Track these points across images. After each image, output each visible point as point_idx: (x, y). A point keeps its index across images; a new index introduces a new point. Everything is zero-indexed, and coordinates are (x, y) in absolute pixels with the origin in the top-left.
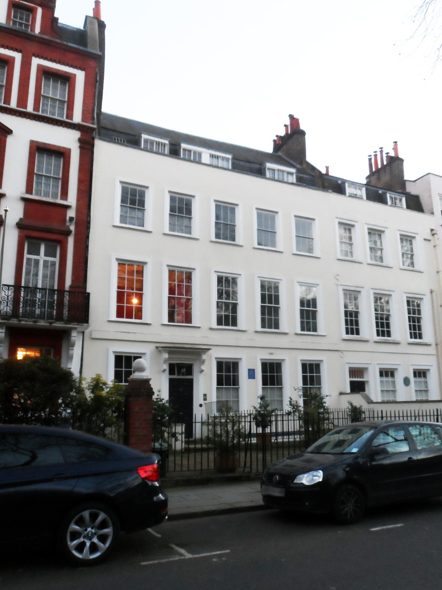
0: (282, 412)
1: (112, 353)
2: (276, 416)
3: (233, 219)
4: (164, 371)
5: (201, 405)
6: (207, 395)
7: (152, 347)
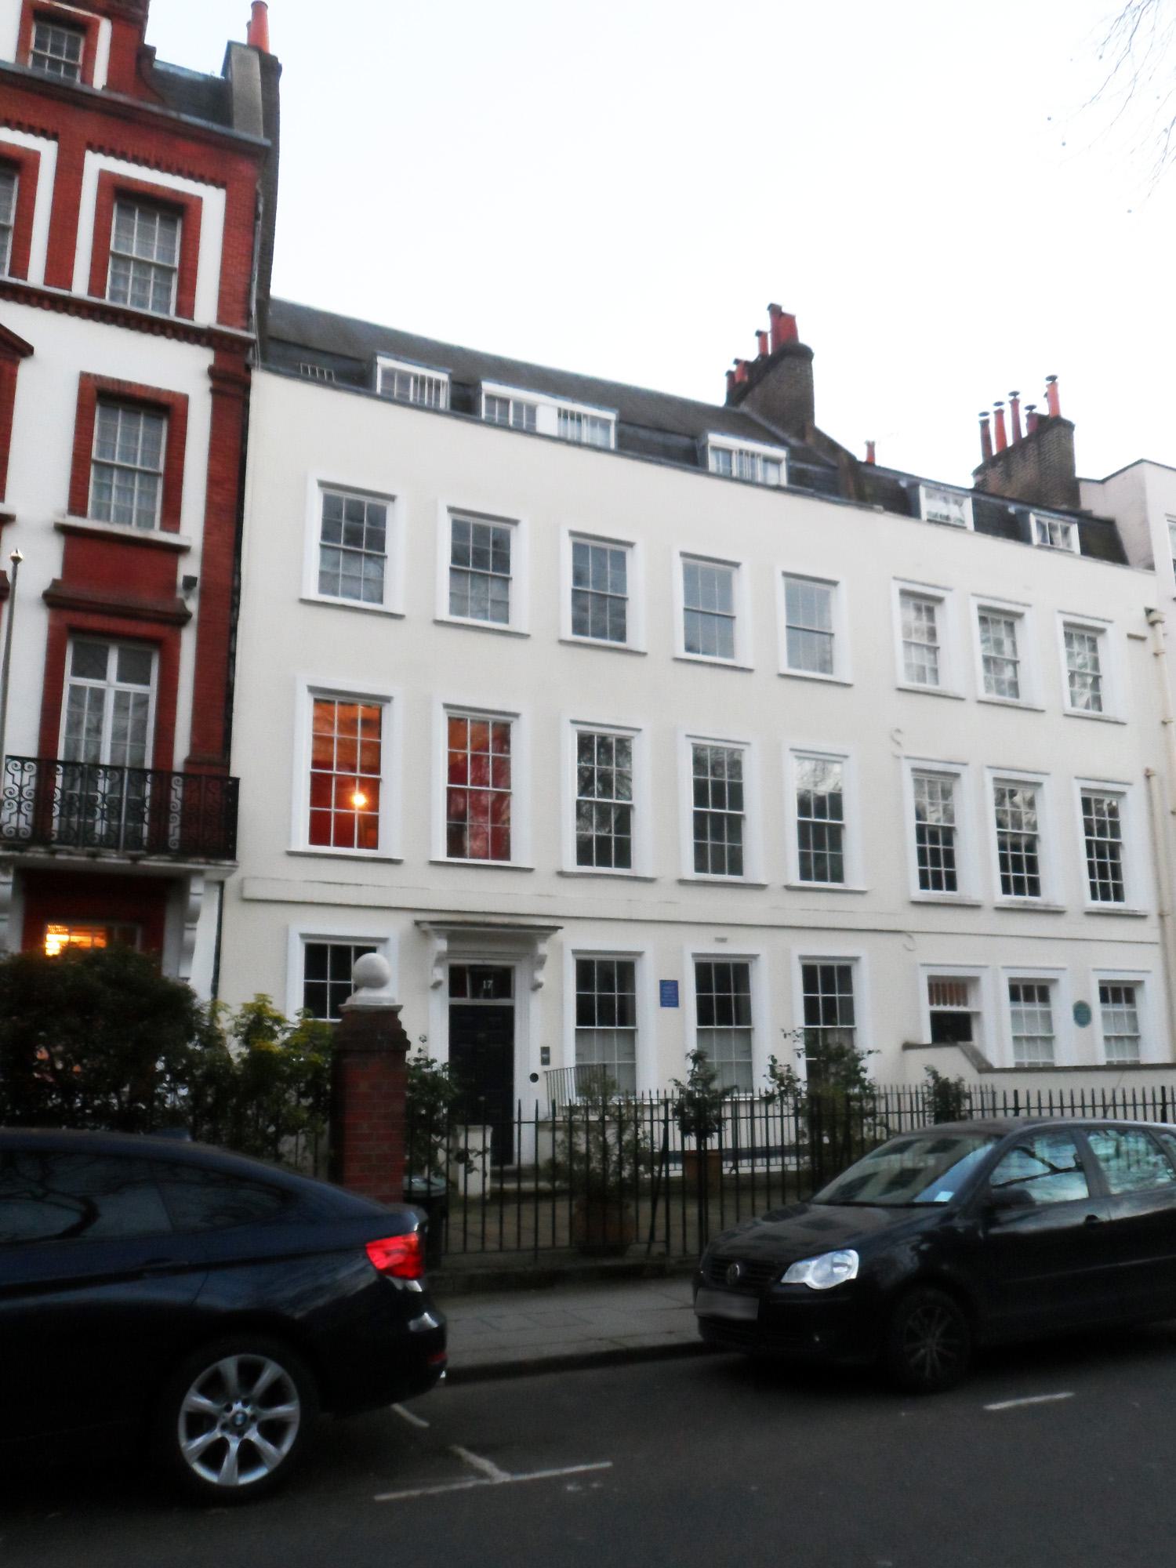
0: (750, 1095)
1: (298, 938)
2: (736, 1105)
3: (620, 582)
4: (437, 985)
5: (534, 1078)
6: (551, 1050)
7: (405, 921)
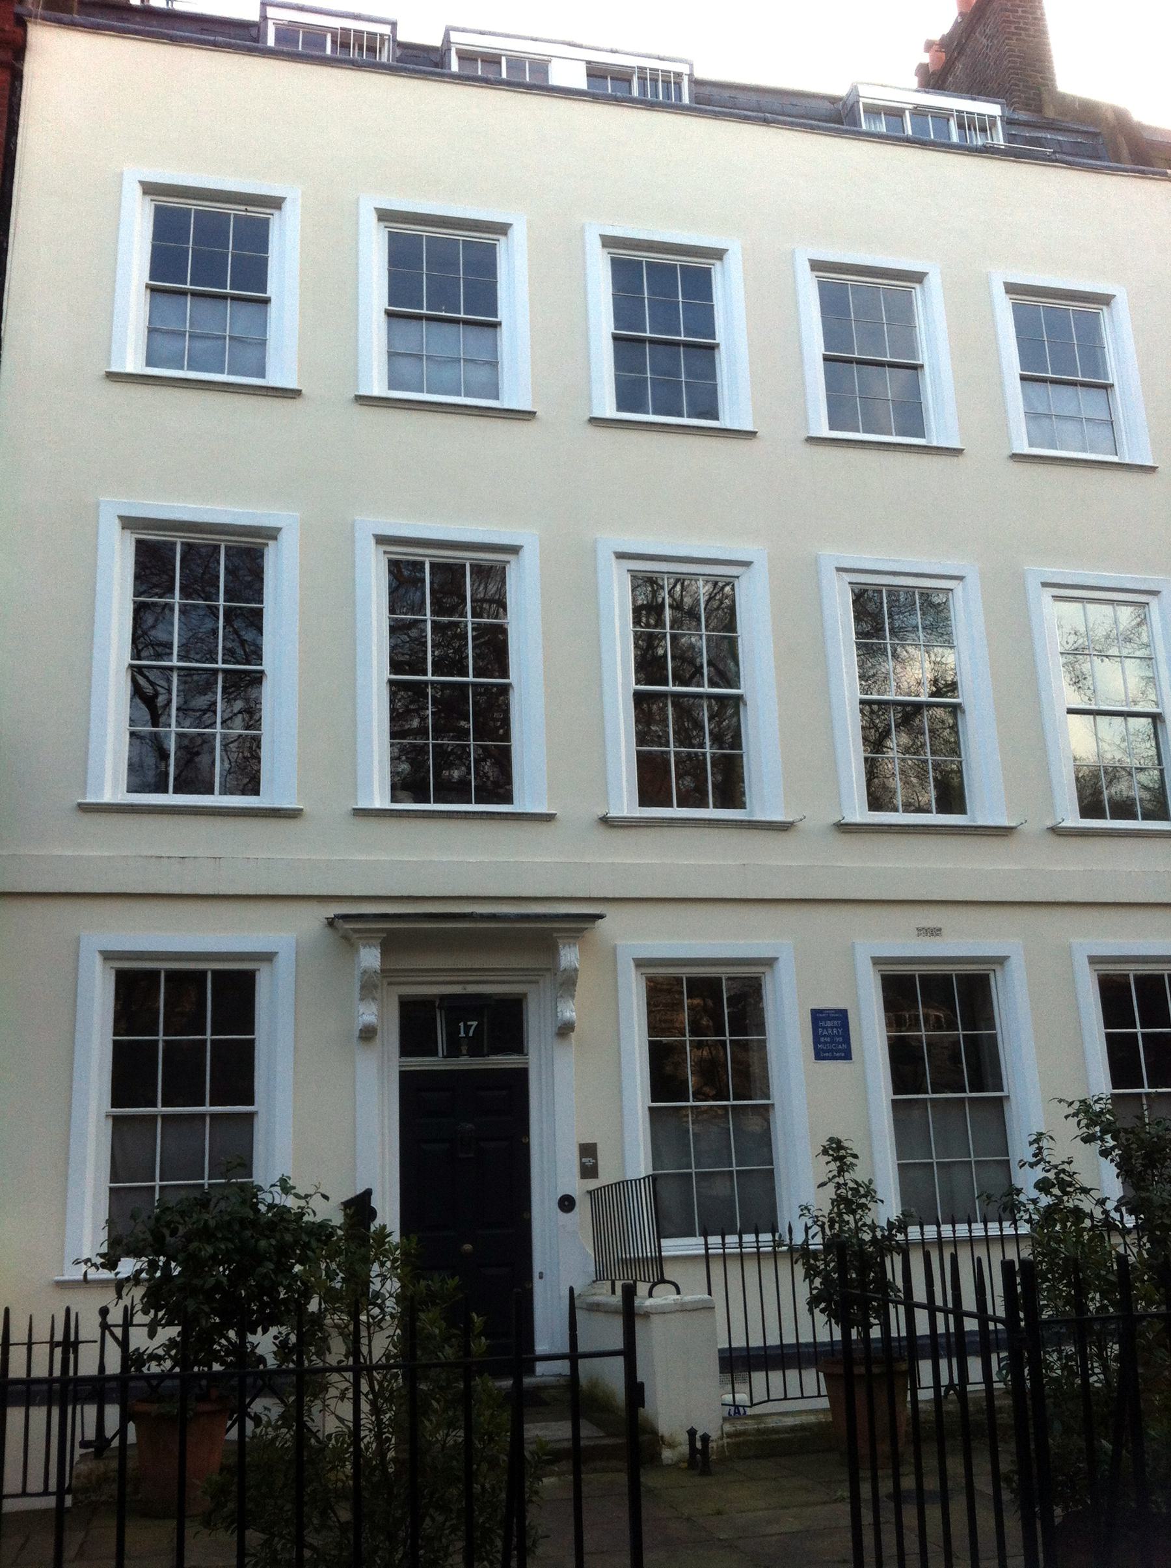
0: (766, 1237)
1: (98, 960)
2: (904, 1250)
3: (704, 320)
4: (368, 1034)
5: (567, 1204)
6: (599, 1147)
7: (312, 919)
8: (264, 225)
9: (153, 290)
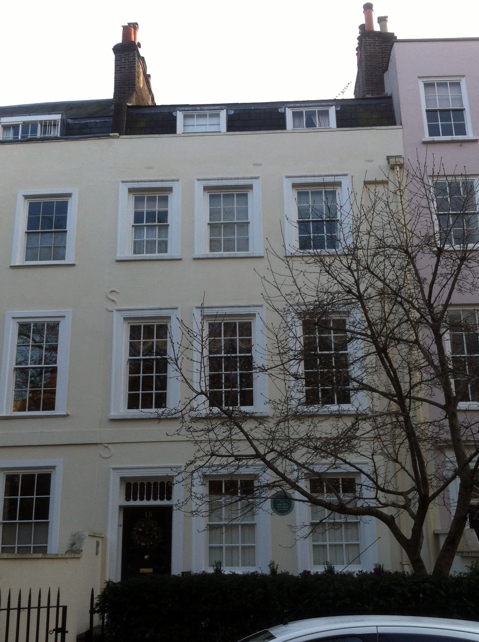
8: (66, 203)
9: (28, 233)
